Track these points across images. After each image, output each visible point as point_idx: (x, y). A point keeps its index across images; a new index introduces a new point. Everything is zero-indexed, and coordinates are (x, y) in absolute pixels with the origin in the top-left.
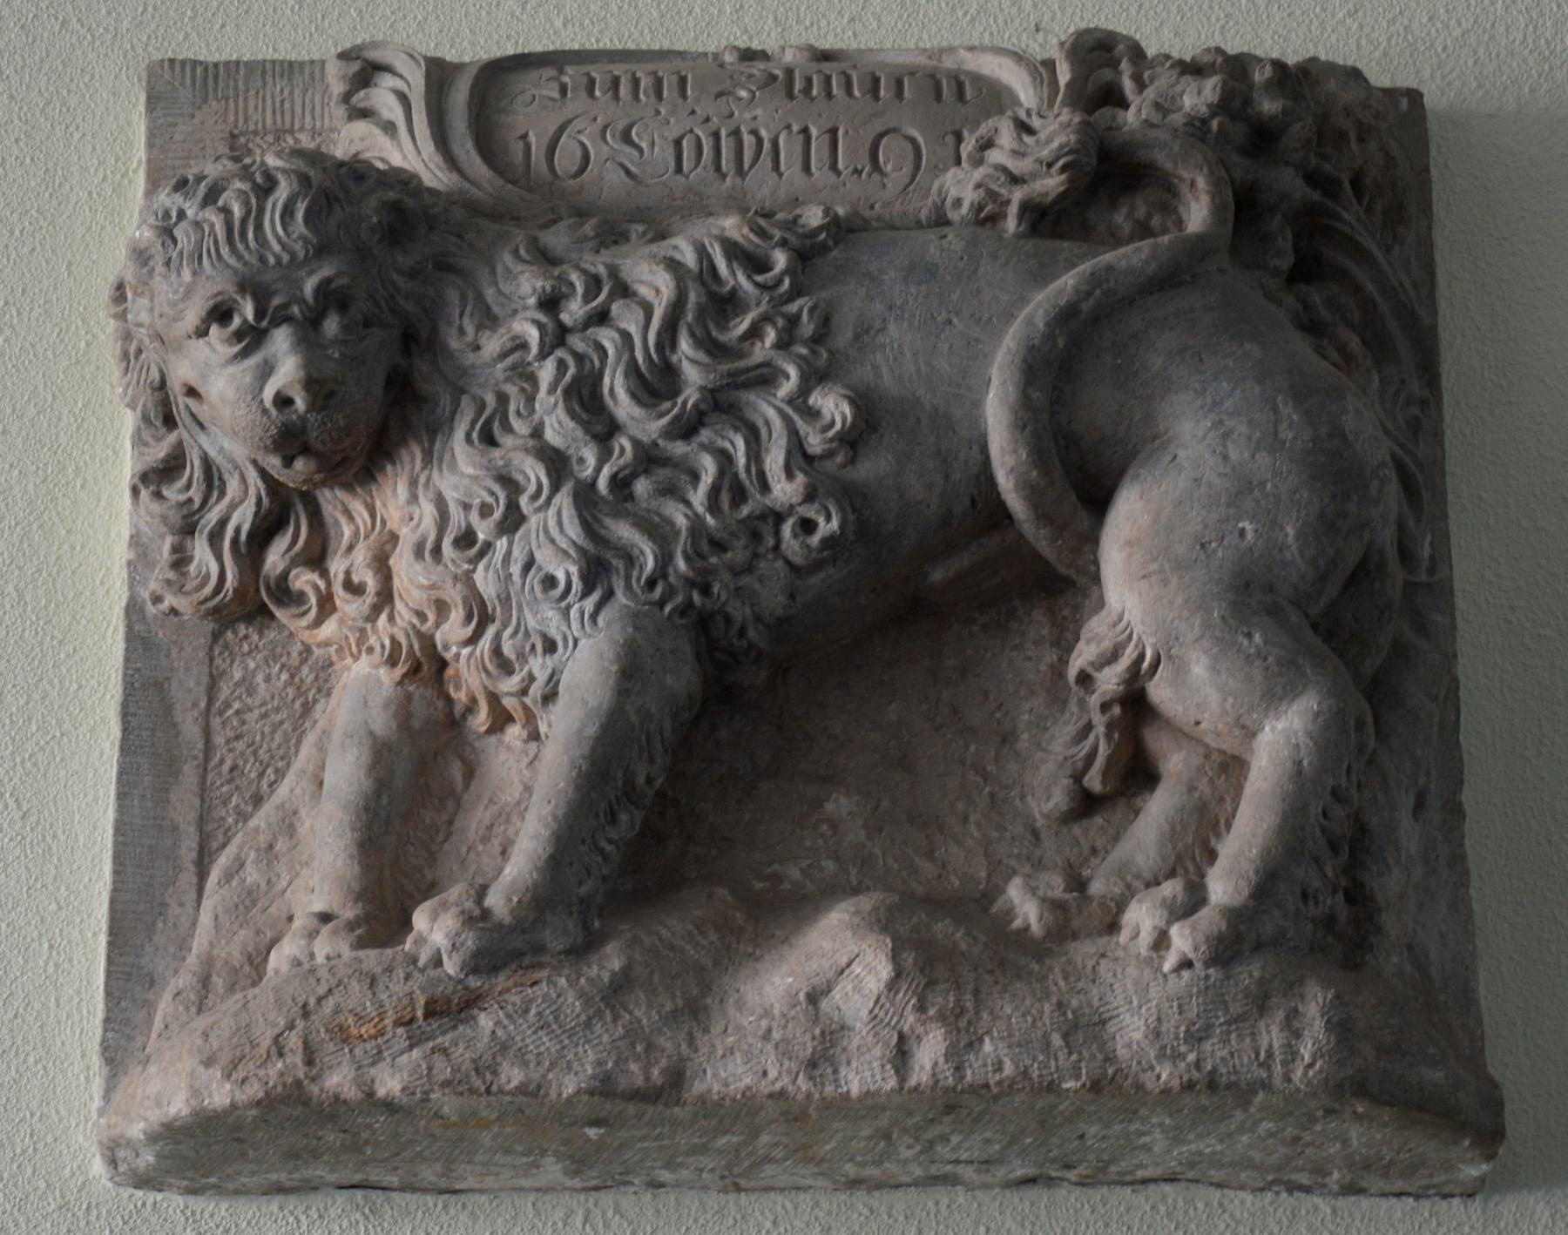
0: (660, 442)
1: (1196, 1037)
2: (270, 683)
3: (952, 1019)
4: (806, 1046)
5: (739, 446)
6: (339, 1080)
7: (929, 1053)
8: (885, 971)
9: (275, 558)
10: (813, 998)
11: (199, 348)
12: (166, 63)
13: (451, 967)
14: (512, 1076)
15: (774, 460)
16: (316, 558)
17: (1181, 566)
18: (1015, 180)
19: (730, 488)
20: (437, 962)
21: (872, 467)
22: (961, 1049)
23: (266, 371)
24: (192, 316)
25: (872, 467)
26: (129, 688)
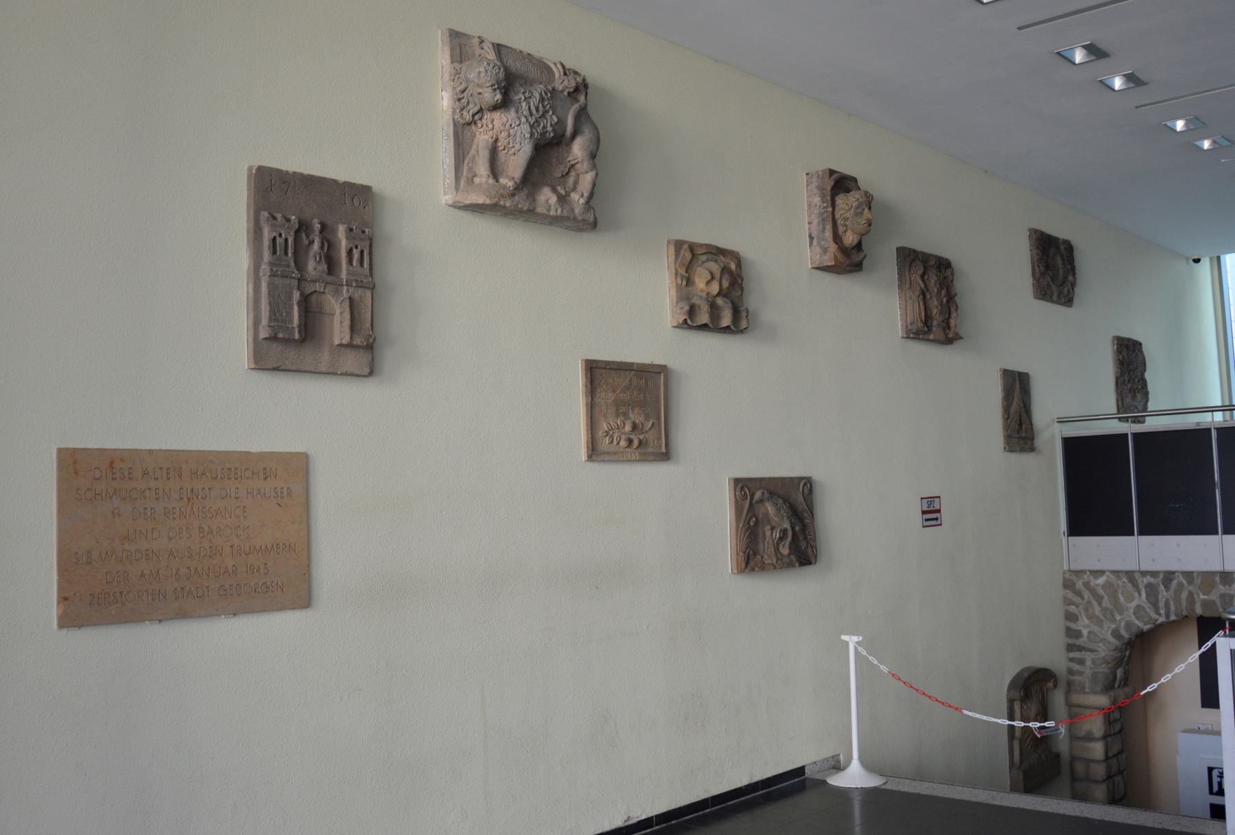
0: (1186, 584)
1: (583, 214)
2: (469, 134)
3: (561, 207)
4: (548, 208)
5: (545, 121)
6: (502, 203)
7: (559, 210)
8: (556, 199)
9: (476, 117)
10: (548, 200)
11: (486, 89)
12: (1072, 655)
13: (511, 188)
14: (520, 206)
15: (549, 125)
16: (481, 119)
17: (586, 150)
18: (567, 88)
19: (544, 127)
20: (509, 187)
21: (557, 128)
22: (562, 211)
23: (496, 95)
24: (488, 84)
25: (557, 128)
26: (454, 133)
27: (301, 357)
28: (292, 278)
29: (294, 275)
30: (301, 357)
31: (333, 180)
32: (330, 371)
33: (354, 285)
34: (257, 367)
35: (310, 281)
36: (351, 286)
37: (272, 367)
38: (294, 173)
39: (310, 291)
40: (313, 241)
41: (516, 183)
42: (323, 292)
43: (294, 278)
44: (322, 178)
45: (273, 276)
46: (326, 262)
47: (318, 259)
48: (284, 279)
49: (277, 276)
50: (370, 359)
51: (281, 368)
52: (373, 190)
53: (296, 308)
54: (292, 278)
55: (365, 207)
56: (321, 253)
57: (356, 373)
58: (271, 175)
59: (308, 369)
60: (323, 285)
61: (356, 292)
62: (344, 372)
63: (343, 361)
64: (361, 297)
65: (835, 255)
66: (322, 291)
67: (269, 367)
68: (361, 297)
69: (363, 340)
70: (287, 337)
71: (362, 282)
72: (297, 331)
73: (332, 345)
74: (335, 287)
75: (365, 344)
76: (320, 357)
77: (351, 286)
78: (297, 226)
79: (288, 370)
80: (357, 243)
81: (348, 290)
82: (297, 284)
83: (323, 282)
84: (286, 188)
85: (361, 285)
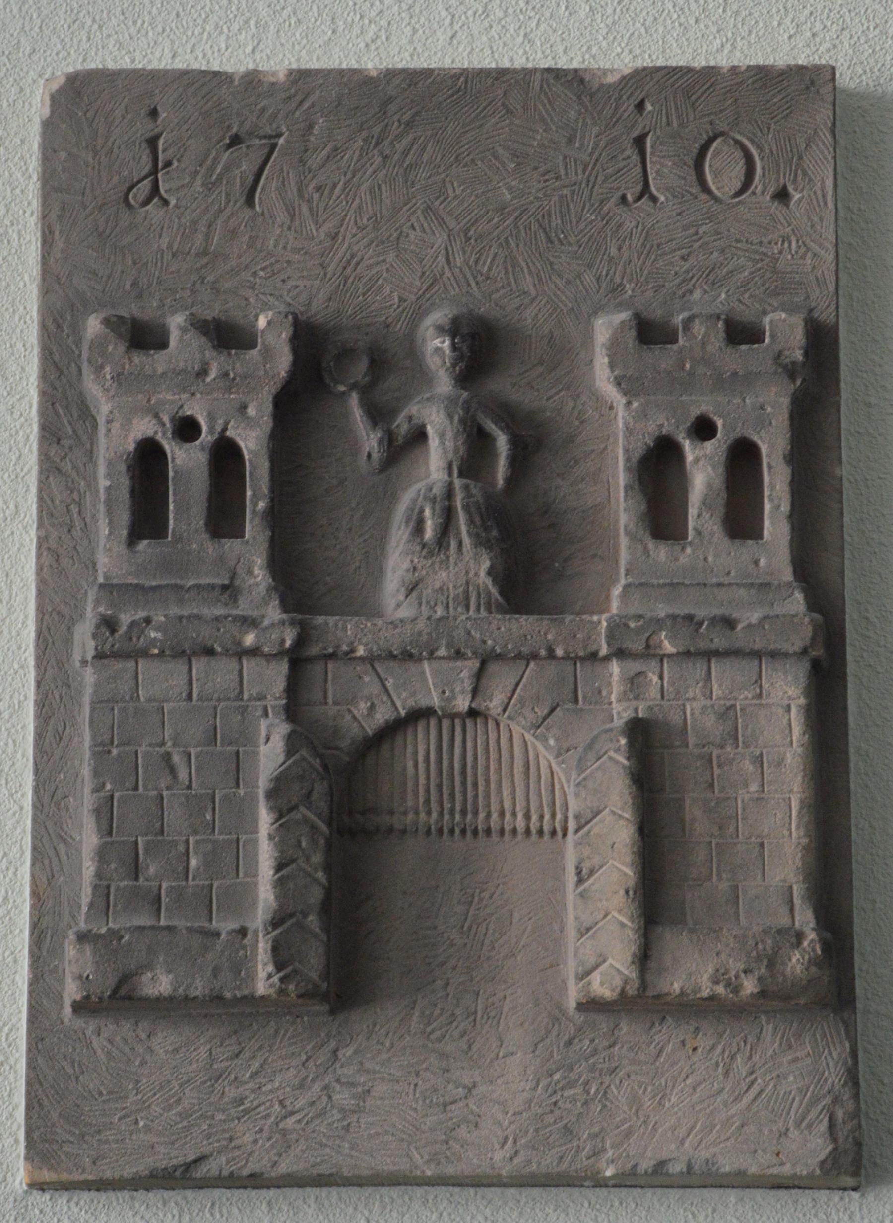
27: (342, 1097)
28: (242, 653)
29: (249, 639)
30: (342, 1097)
31: (555, 73)
32: (547, 1162)
33: (669, 648)
34: (47, 1175)
35: (370, 660)
36: (650, 652)
37: (141, 1168)
38: (300, 76)
39: (382, 716)
40: (419, 436)
41: (324, 888)
42: (473, 713)
43: (254, 652)
44: (483, 73)
45: (116, 655)
46: (480, 542)
47: (429, 533)
48: (199, 665)
49: (144, 653)
50: (835, 1077)
51: (201, 1172)
52: (845, 79)
53: (265, 819)
54: (242, 653)
55: (782, 195)
56: (449, 494)
57: (727, 1166)
58: (154, 113)
59: (385, 1164)
60: (467, 669)
61: (695, 691)
62: (646, 1165)
63: (634, 1101)
64: (727, 713)
65: (667, 994)
66: (463, 703)
67: (128, 1172)
68: (727, 713)
69: (735, 966)
70: (199, 988)
71: (729, 623)
72: (263, 947)
73: (557, 1016)
74: (551, 669)
75: (749, 986)
76: (470, 1090)
77: (650, 652)
78: (283, 362)
79: (478, 1182)
80: (703, 405)
81: (634, 683)
82: (279, 685)
83: (459, 655)
84: (247, 167)
85: (719, 642)
